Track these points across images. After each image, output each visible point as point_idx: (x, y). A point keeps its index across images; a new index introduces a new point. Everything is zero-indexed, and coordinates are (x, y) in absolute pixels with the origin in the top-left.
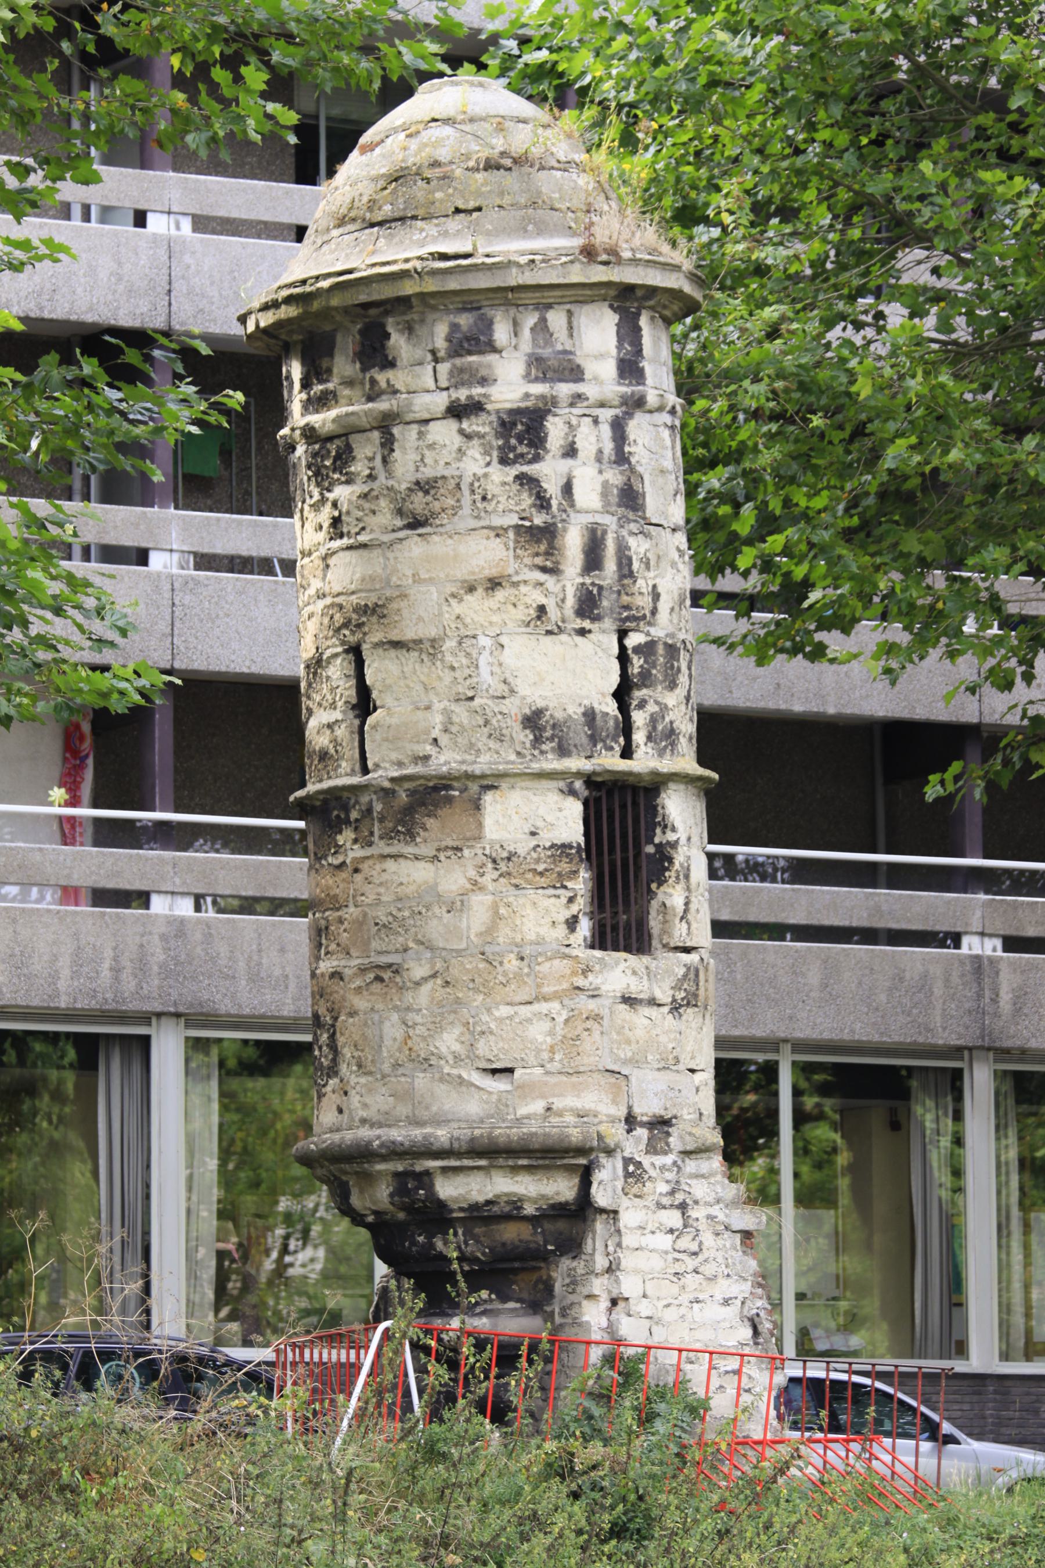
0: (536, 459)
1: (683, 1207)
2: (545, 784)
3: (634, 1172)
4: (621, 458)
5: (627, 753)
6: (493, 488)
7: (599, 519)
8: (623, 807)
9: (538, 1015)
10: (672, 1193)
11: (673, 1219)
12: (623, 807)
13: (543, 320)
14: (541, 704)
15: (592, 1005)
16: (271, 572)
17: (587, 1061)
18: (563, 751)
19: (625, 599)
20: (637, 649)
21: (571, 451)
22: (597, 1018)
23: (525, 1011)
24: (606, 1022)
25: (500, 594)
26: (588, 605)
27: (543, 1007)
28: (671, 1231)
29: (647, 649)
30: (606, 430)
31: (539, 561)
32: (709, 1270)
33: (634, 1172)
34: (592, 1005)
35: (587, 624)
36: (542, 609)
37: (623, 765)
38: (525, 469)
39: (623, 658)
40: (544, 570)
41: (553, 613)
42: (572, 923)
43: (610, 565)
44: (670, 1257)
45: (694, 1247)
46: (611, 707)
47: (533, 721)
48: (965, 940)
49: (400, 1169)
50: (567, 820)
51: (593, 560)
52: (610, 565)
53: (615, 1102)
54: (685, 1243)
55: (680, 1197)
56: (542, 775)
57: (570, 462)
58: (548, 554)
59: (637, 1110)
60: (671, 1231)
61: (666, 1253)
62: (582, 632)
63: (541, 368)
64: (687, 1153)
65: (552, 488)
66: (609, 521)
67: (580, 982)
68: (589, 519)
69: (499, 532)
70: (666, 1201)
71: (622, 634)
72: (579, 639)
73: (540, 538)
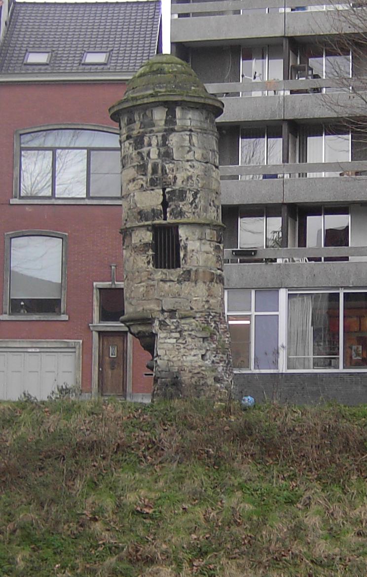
0: (142, 148)
1: (180, 332)
2: (142, 229)
3: (163, 324)
4: (164, 144)
5: (165, 219)
6: (133, 156)
7: (157, 161)
8: (165, 235)
9: (141, 286)
10: (176, 328)
11: (178, 335)
12: (165, 235)
13: (145, 113)
14: (142, 208)
15: (152, 283)
16: (193, 13)
17: (150, 297)
18: (147, 220)
19: (164, 180)
20: (168, 192)
21: (150, 145)
22: (153, 286)
23: (139, 285)
24: (156, 287)
25: (135, 182)
26: (153, 183)
27: (142, 284)
28: (176, 338)
29: (173, 192)
30: (160, 138)
31: (142, 173)
32: (190, 347)
33: (163, 324)
34: (152, 283)
35: (153, 188)
36: (142, 185)
37: (164, 222)
38: (139, 150)
39: (164, 195)
40: (143, 175)
41: (145, 185)
42: (149, 263)
43: (160, 171)
44: (175, 345)
45: (184, 342)
46: (160, 207)
47: (140, 213)
48: (278, 260)
49: (360, 336)
50: (148, 237)
51: (155, 171)
52: (160, 171)
53: (158, 307)
54: (180, 341)
55: (179, 330)
56: (143, 226)
57: (149, 148)
58: (144, 171)
59: (164, 308)
60: (176, 338)
61: (174, 343)
62: (153, 190)
63: (143, 125)
64: (182, 318)
65: (145, 155)
66: (159, 161)
67: (149, 277)
68: (154, 161)
69: (134, 167)
70: (174, 331)
71: (164, 190)
72: (152, 192)
73: (142, 168)
